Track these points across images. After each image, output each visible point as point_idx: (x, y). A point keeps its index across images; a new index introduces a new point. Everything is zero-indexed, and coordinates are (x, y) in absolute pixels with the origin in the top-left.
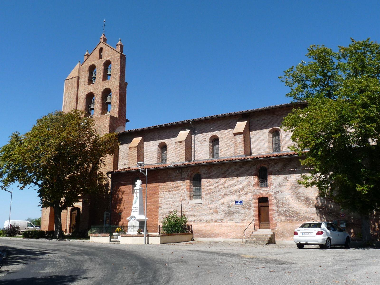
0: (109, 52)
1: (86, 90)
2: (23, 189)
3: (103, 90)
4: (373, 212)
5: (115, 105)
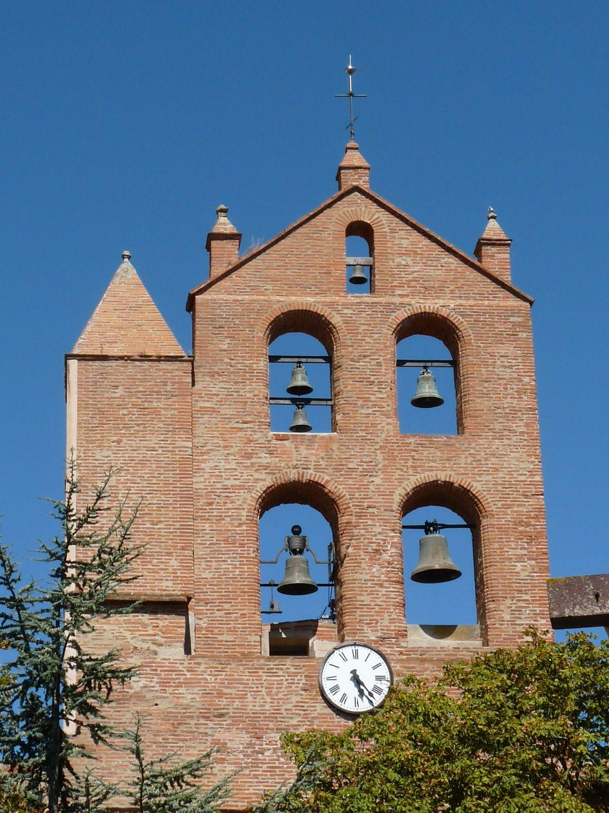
0: (425, 264)
1: (264, 458)
2: (68, 551)
3: (442, 476)
4: (110, 594)
5: (525, 597)
